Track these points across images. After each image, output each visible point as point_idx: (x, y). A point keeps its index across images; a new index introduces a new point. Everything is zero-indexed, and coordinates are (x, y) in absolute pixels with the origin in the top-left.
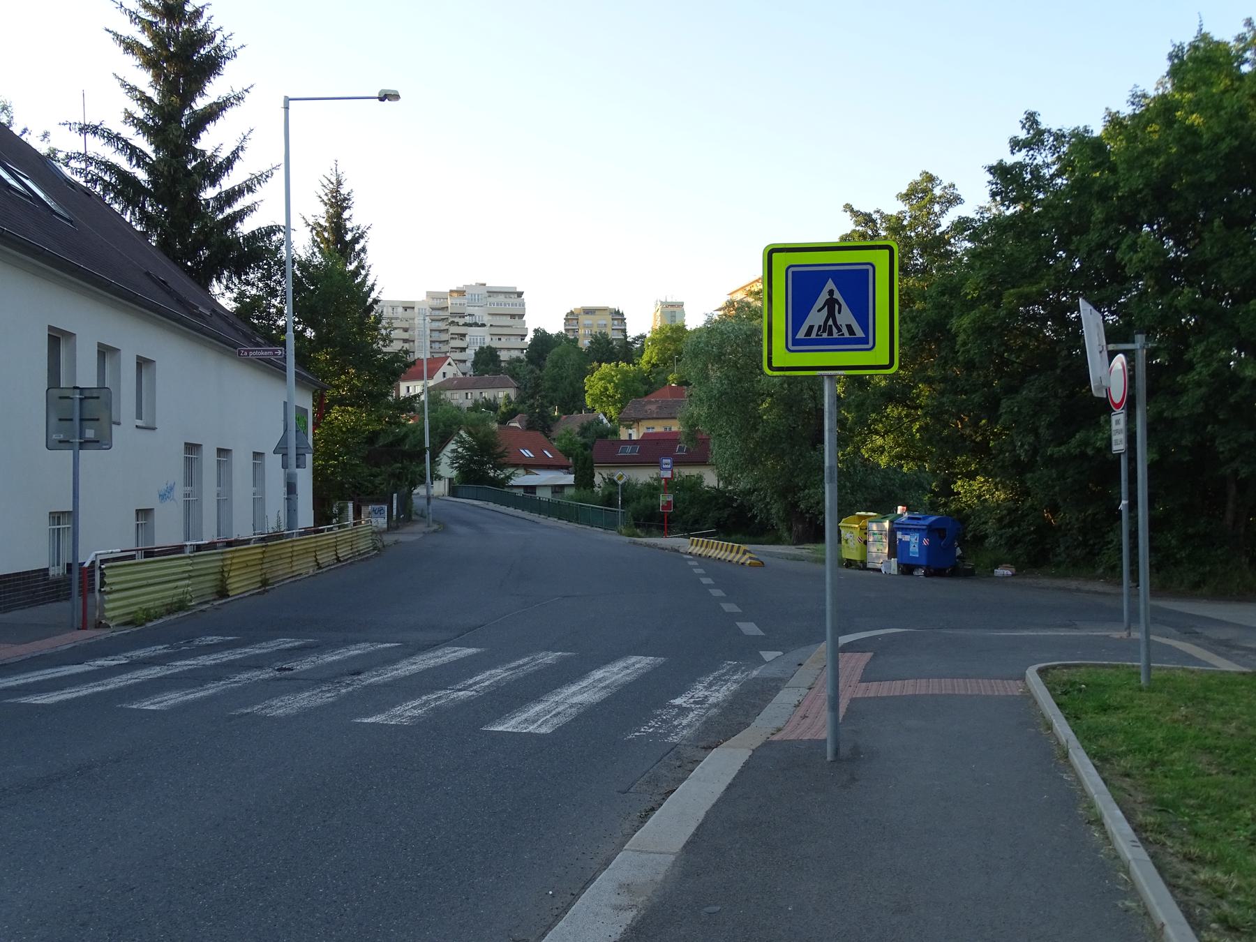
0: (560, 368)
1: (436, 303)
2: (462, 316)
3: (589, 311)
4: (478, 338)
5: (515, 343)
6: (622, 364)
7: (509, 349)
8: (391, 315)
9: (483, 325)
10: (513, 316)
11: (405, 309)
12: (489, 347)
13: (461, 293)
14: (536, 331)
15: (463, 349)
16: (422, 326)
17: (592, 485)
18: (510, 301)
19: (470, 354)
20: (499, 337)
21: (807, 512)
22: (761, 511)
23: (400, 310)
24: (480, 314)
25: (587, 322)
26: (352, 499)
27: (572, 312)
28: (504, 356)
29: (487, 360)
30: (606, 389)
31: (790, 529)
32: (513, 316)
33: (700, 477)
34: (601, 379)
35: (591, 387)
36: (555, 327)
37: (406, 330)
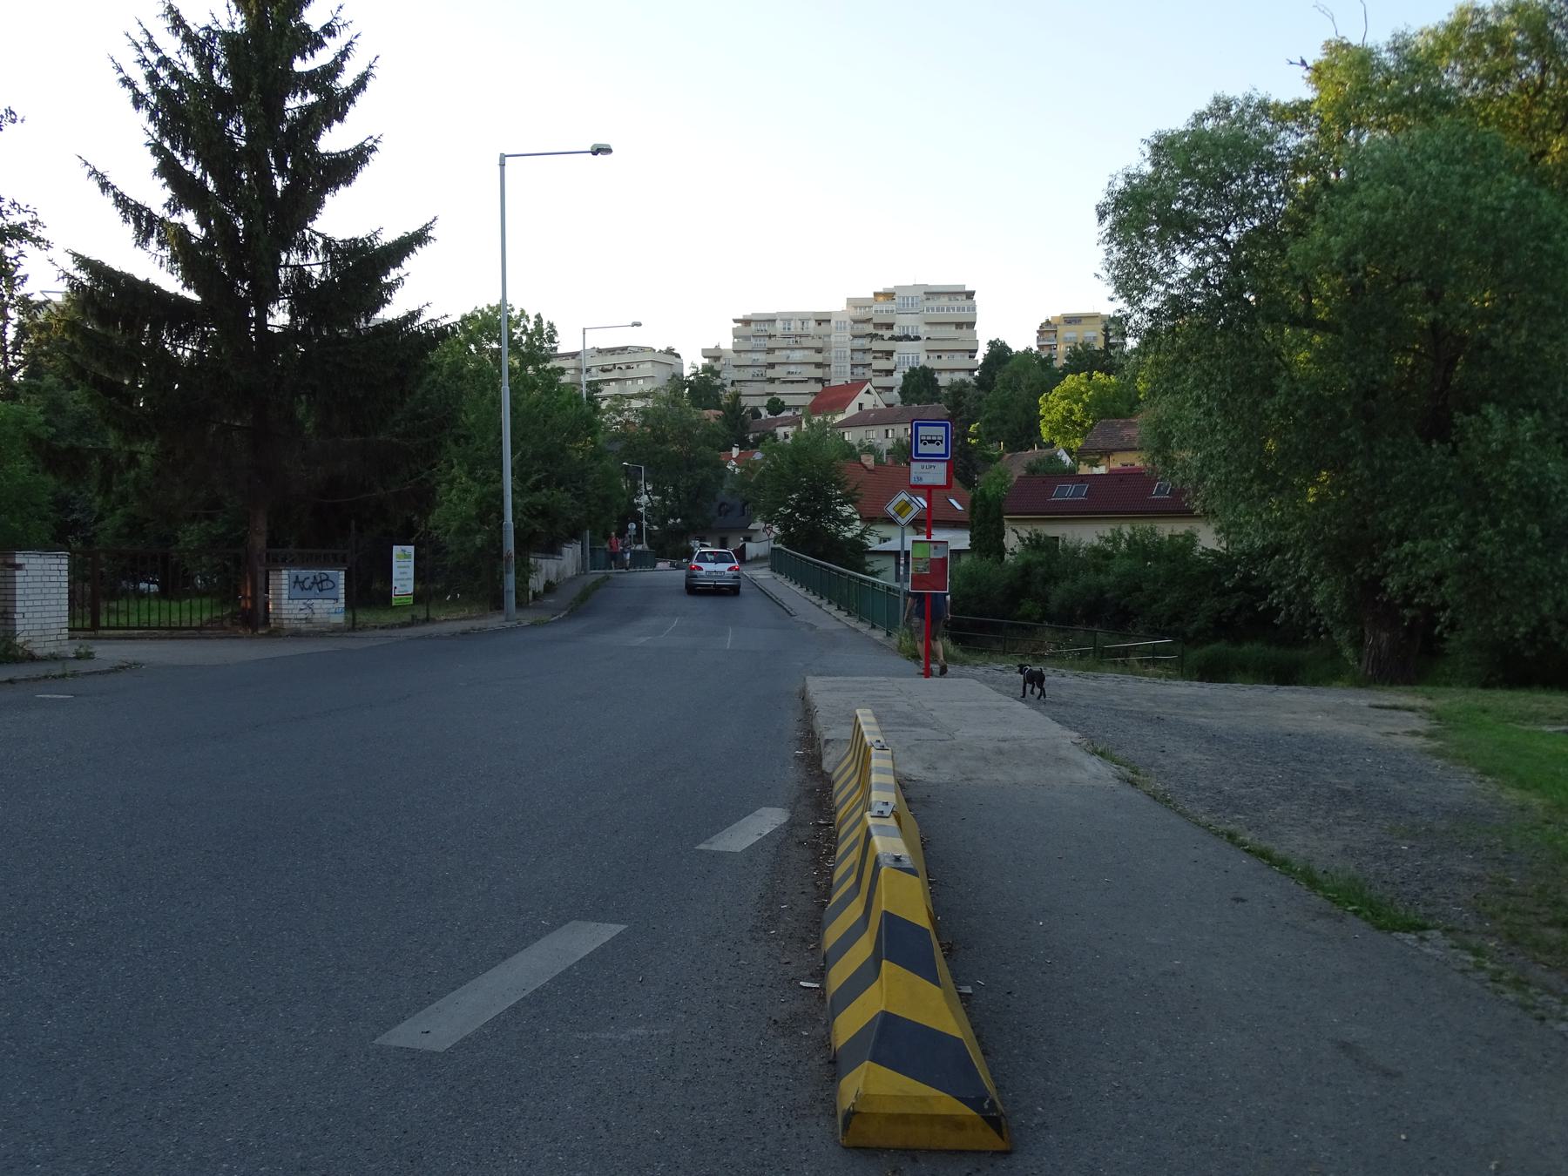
0: (1015, 389)
1: (859, 314)
2: (890, 326)
3: (1071, 320)
4: (910, 356)
5: (962, 361)
6: (1097, 375)
7: (952, 371)
8: (799, 331)
9: (917, 338)
10: (959, 325)
11: (819, 322)
12: (924, 368)
13: (889, 295)
14: (992, 344)
15: (889, 372)
16: (841, 340)
17: (1001, 550)
18: (954, 304)
19: (898, 378)
20: (939, 353)
21: (1408, 602)
22: (1289, 601)
23: (812, 324)
24: (904, 323)
25: (1068, 335)
26: (55, 541)
27: (1048, 323)
28: (943, 380)
29: (920, 383)
30: (1071, 412)
31: (1358, 643)
32: (959, 325)
33: (1191, 538)
34: (1063, 398)
35: (1048, 411)
36: (1022, 340)
37: (819, 351)
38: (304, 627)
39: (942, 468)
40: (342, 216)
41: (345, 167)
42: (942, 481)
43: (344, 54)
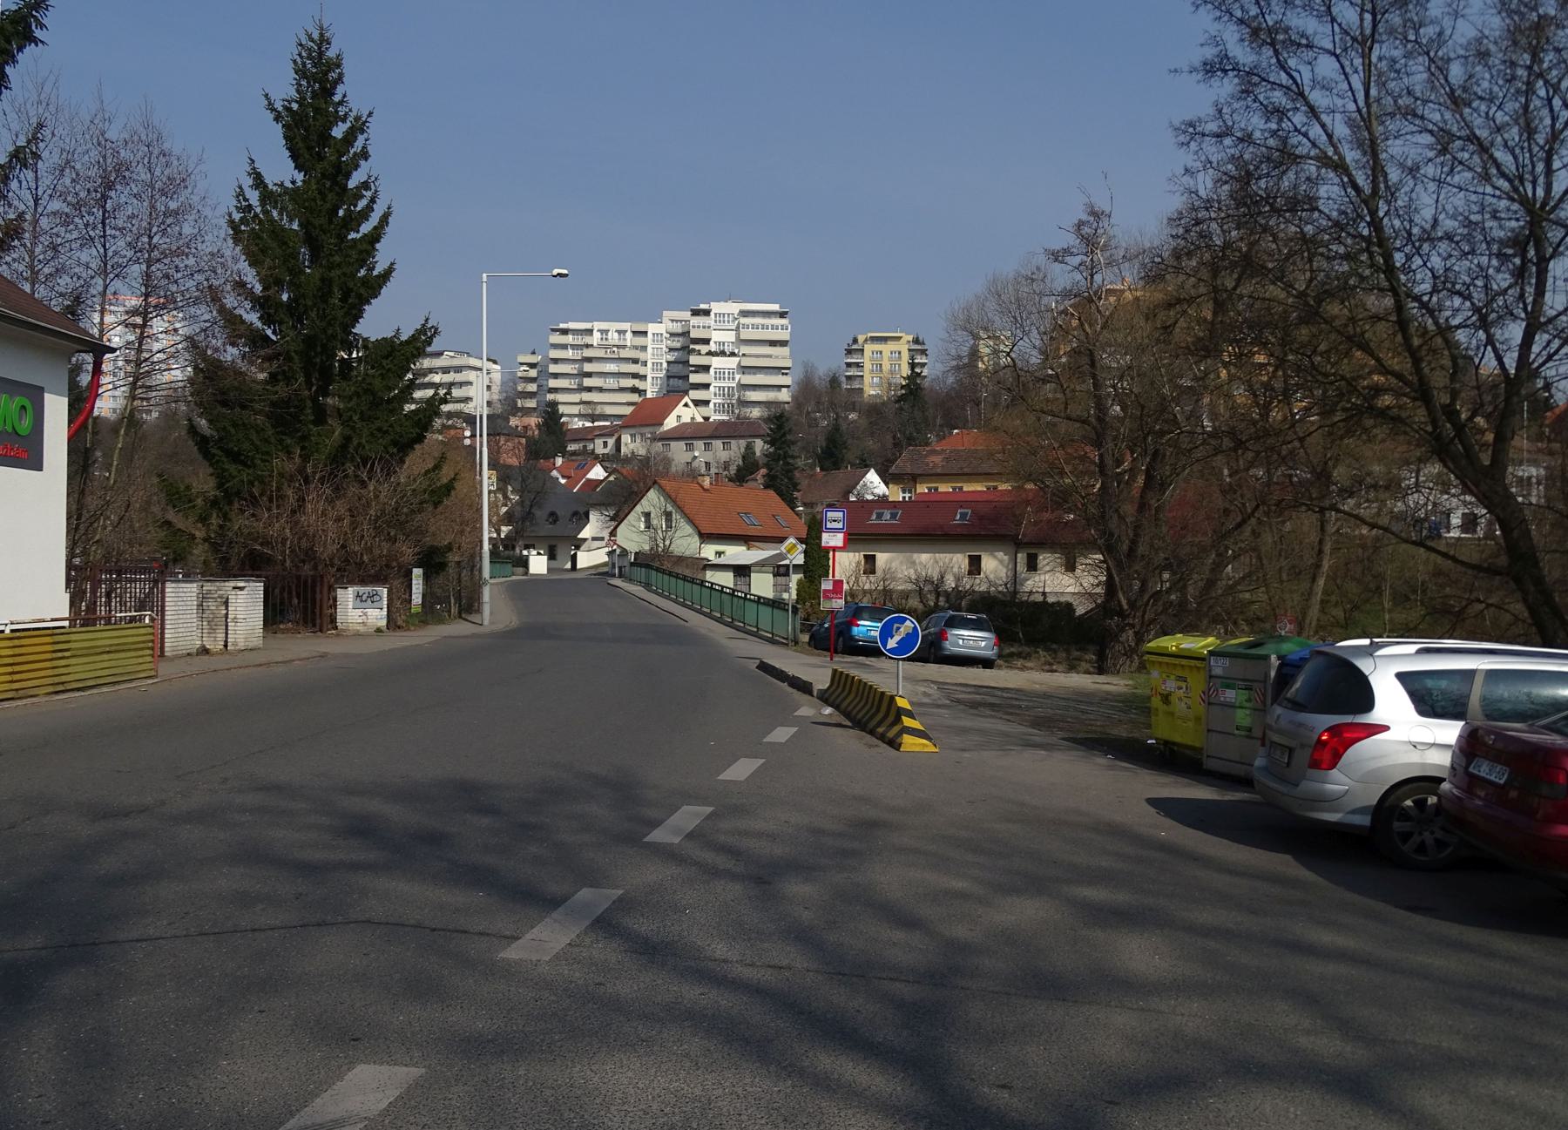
2: (707, 341)
38: (361, 629)
39: (841, 536)
40: (376, 323)
41: (374, 286)
42: (840, 544)
43: (373, 201)
